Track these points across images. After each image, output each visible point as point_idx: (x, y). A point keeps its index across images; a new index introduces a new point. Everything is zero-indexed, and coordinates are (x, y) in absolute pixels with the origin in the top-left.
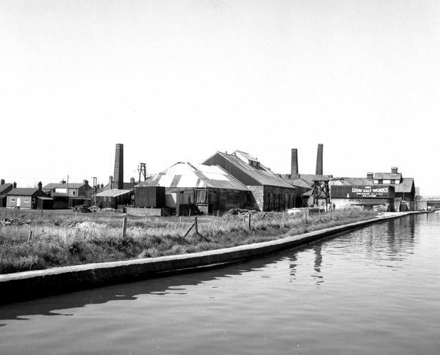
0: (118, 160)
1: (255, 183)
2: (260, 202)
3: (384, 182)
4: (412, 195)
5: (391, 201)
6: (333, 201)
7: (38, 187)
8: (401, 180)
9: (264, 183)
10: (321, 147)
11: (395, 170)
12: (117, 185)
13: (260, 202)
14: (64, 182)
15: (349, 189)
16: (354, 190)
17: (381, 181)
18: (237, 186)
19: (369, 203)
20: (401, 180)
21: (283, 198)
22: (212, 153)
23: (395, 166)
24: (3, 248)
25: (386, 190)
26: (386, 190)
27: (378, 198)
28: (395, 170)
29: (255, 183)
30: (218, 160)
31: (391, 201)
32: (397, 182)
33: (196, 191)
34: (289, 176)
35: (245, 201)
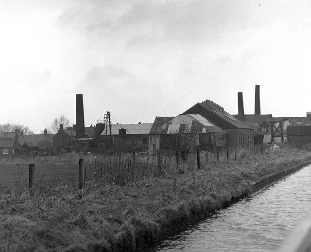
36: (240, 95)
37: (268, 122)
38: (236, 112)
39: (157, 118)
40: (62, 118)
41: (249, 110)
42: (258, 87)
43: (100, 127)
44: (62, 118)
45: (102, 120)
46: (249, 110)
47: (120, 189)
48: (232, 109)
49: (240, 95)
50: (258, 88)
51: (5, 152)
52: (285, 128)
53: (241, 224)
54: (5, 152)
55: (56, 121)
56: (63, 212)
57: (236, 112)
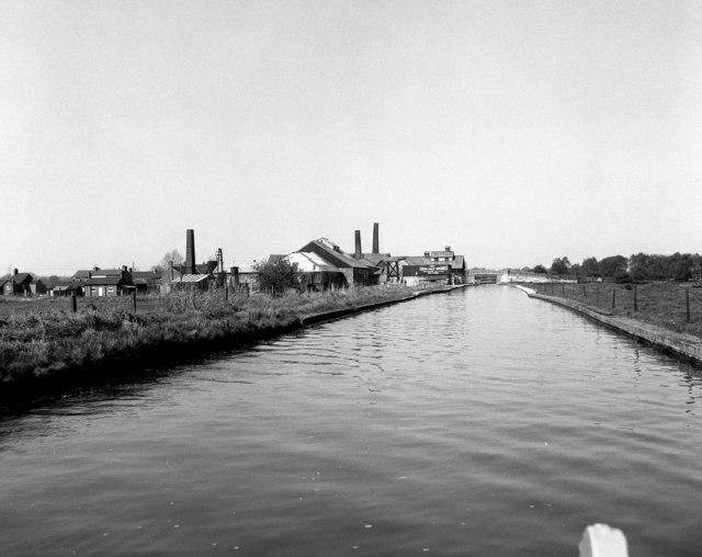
0: (190, 254)
1: (347, 266)
2: (350, 280)
3: (440, 260)
4: (462, 271)
5: (450, 276)
6: (405, 278)
7: (13, 274)
8: (454, 258)
9: (353, 265)
10: (376, 226)
11: (448, 249)
12: (189, 270)
13: (350, 280)
14: (97, 269)
15: (417, 267)
16: (422, 269)
17: (437, 259)
18: (332, 269)
19: (433, 279)
20: (454, 258)
21: (367, 277)
22: (305, 243)
23: (448, 245)
24: (4, 330)
25: (446, 268)
26: (446, 268)
27: (440, 274)
28: (448, 249)
29: (347, 266)
30: (313, 247)
31: (450, 276)
32: (451, 259)
33: (314, 275)
34: (354, 256)
35: (340, 280)
36: (358, 234)
37: (385, 264)
38: (353, 251)
39: (272, 256)
40: (175, 253)
41: (367, 248)
42: (376, 226)
43: (213, 264)
44: (175, 253)
45: (214, 258)
46: (367, 248)
47: (71, 316)
48: (348, 248)
49: (358, 234)
50: (376, 226)
51: (8, 288)
52: (400, 267)
53: (350, 285)
54: (8, 288)
55: (167, 256)
56: (378, 275)
57: (353, 251)
